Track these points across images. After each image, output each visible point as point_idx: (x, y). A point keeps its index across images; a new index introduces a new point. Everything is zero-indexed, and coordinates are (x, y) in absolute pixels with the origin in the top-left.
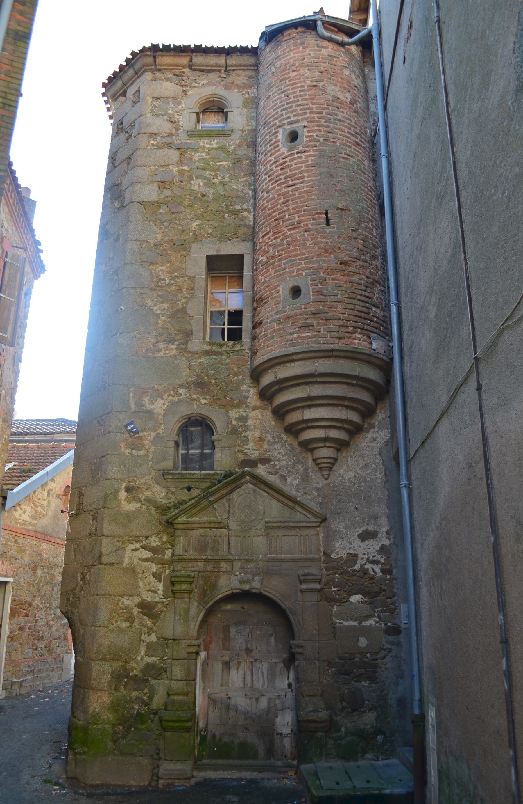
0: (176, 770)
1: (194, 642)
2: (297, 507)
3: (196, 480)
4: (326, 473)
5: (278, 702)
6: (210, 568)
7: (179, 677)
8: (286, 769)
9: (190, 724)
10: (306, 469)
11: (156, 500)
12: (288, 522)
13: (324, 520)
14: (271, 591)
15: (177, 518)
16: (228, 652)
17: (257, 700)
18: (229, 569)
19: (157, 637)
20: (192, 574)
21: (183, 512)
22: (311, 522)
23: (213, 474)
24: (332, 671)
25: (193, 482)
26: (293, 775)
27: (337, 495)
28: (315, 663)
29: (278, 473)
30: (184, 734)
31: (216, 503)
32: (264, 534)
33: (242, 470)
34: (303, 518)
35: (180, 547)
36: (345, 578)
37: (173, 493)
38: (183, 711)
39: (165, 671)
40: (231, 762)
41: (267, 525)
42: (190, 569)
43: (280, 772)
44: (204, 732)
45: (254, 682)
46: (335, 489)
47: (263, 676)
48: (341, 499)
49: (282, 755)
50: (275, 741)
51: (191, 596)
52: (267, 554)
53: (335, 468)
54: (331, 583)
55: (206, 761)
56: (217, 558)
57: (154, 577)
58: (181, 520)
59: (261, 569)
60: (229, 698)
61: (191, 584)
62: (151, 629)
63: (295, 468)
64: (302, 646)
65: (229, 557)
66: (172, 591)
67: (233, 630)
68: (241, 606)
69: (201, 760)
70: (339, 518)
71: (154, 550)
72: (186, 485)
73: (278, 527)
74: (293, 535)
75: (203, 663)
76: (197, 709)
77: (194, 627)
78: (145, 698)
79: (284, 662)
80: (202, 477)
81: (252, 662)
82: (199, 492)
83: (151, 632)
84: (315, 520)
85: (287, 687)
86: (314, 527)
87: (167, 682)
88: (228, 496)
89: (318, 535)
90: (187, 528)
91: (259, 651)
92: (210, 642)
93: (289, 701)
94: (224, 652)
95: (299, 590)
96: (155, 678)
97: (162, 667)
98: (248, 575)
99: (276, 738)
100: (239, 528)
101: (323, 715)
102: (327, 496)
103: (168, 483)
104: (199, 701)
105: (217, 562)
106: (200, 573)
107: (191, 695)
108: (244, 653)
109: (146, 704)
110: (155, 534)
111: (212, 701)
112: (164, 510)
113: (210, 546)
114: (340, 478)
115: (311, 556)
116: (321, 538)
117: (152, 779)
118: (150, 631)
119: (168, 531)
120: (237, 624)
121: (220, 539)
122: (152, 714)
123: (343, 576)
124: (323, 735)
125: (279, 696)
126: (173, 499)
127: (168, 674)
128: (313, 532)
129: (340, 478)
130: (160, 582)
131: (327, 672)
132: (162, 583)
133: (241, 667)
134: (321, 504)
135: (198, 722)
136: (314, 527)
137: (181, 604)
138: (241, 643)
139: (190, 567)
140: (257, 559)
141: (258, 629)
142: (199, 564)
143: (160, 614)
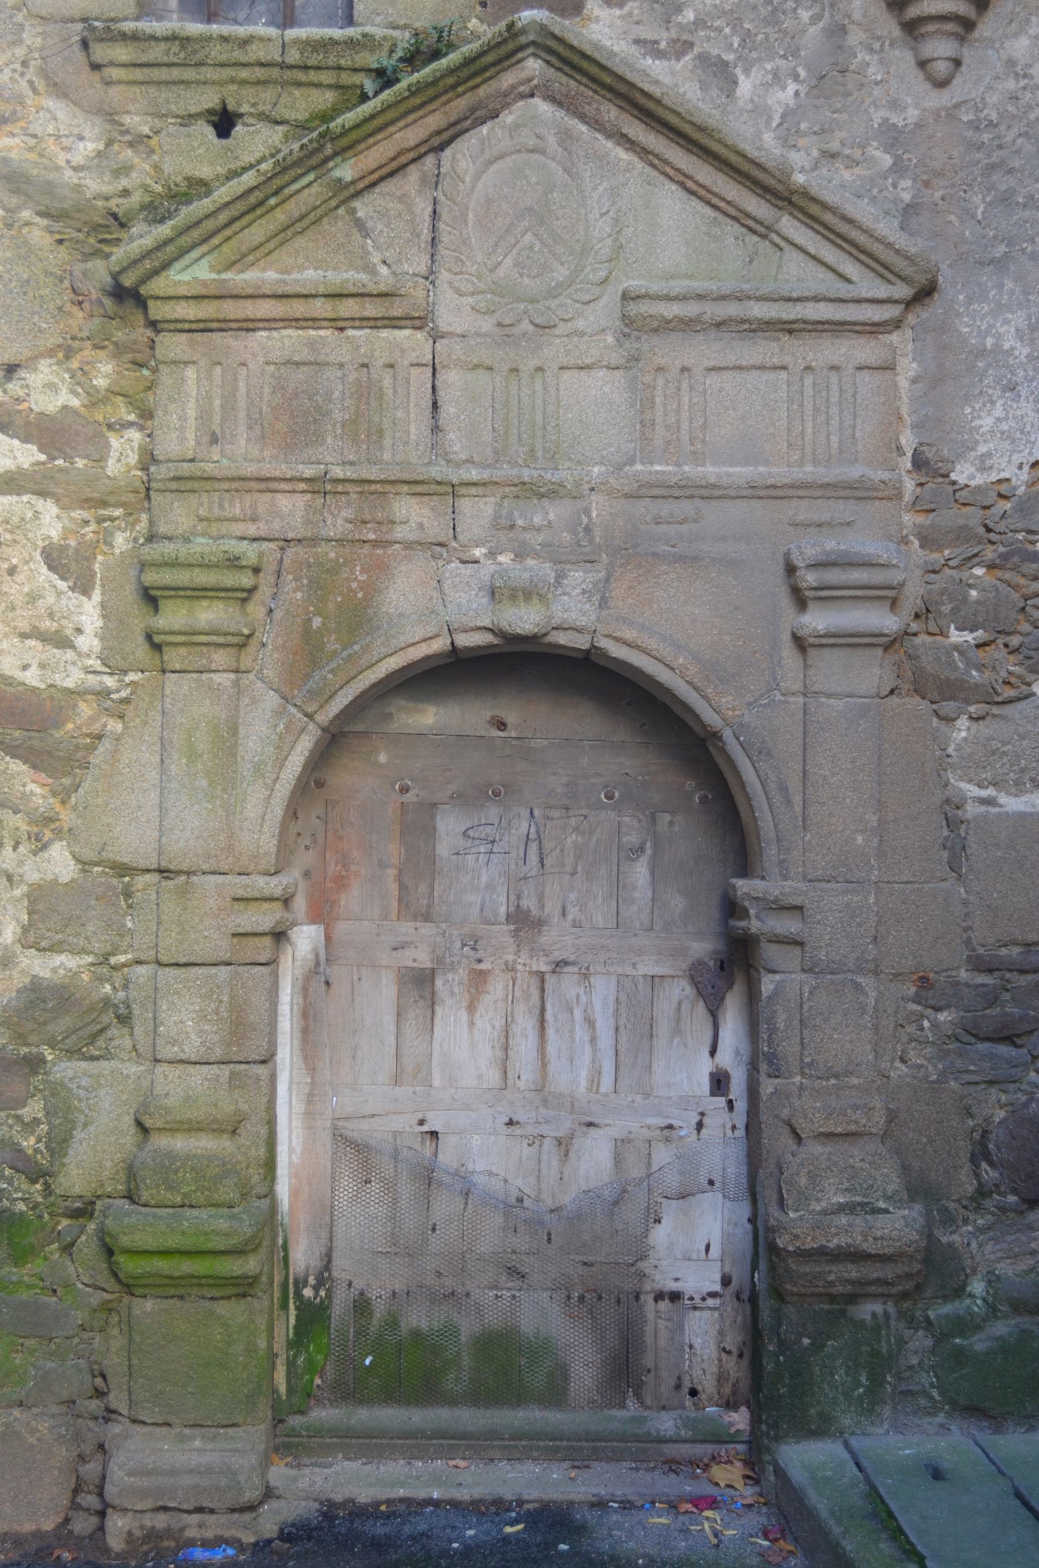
0: (191, 1472)
1: (261, 881)
2: (789, 225)
3: (259, 73)
4: (940, 48)
5: (662, 1155)
6: (337, 522)
7: (192, 1048)
8: (701, 1450)
9: (251, 1265)
10: (838, 31)
11: (52, 176)
12: (741, 297)
13: (926, 293)
14: (652, 643)
15: (166, 266)
16: (427, 930)
17: (564, 1145)
18: (436, 529)
19: (78, 860)
20: (250, 552)
21: (196, 234)
22: (859, 301)
23: (351, 44)
24: (935, 1025)
25: (244, 82)
26: (739, 1484)
27: (992, 167)
28: (858, 987)
29: (689, 45)
30: (222, 1308)
31: (369, 197)
32: (615, 359)
33: (502, 25)
34: (819, 281)
35: (183, 418)
36: (1016, 587)
37: (138, 142)
38: (217, 1205)
39: (124, 1020)
40: (441, 1416)
41: (633, 309)
42: (239, 529)
43: (672, 1466)
44: (316, 1289)
45: (553, 1067)
46: (986, 137)
47: (593, 1040)
48: (1012, 191)
49: (678, 1387)
50: (649, 1329)
51: (246, 662)
52: (632, 462)
53: (985, 29)
54: (946, 608)
55: (323, 1414)
56: (372, 473)
57: (51, 568)
58: (186, 277)
59: (597, 533)
60: (434, 1134)
61: (244, 600)
62: (49, 820)
63: (777, 22)
64: (800, 908)
65: (435, 472)
66: (149, 637)
67: (449, 826)
68: (488, 714)
69: (302, 1412)
70: (1000, 286)
71: (49, 433)
72: (210, 99)
73: (688, 325)
74: (762, 368)
75: (307, 979)
76: (283, 1189)
77: (260, 812)
78: (28, 1143)
79: (695, 975)
80: (293, 56)
81: (541, 976)
82: (275, 135)
83: (48, 835)
84: (882, 291)
85: (705, 1085)
86: (875, 329)
87: (133, 1069)
88: (430, 160)
89: (889, 367)
90: (219, 322)
91: (576, 925)
92: (341, 882)
93: (720, 1150)
94: (407, 928)
95: (786, 637)
96: (74, 1053)
97: (107, 1002)
98: (530, 562)
99: (650, 1315)
100: (486, 324)
101: (898, 1225)
102: (939, 174)
103: (114, 92)
104: (291, 1150)
105: (374, 490)
106: (290, 552)
107: (253, 1130)
108: (502, 933)
109: (36, 1174)
110: (51, 353)
111: (355, 1150)
112: (96, 228)
113: (338, 416)
114: (1011, 84)
115: (855, 472)
116: (904, 383)
117: (75, 1506)
118: (43, 831)
119: (119, 336)
120: (461, 800)
121: (387, 382)
122: (65, 1215)
123: (1008, 575)
124: (887, 1315)
125: (670, 1127)
126: (141, 175)
127: (138, 1031)
128: (865, 350)
129: (1011, 84)
130: (86, 591)
131: (911, 1029)
132: (97, 596)
133: (487, 1000)
134: (910, 210)
135: (285, 1247)
136: (875, 329)
137: (193, 699)
138: (490, 887)
139: (234, 519)
140: (578, 484)
141: (573, 822)
142: (284, 502)
143: (91, 748)
